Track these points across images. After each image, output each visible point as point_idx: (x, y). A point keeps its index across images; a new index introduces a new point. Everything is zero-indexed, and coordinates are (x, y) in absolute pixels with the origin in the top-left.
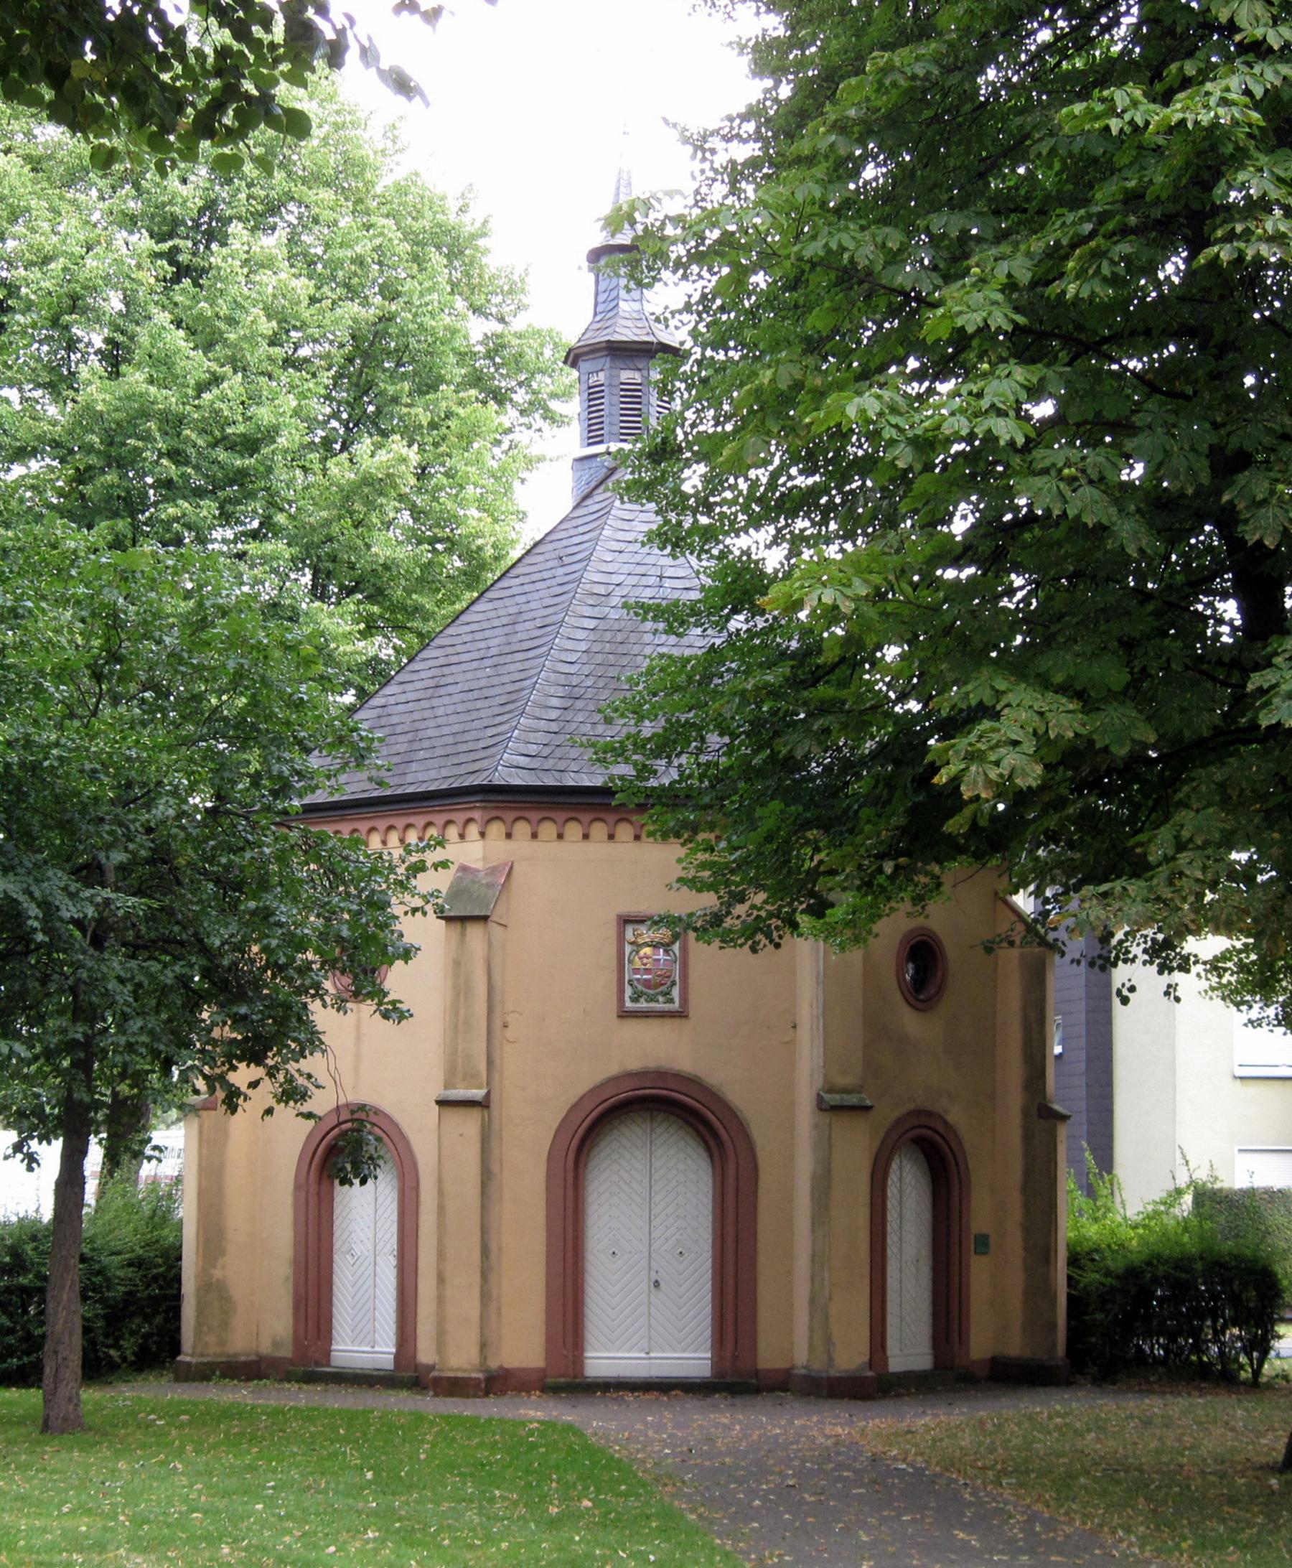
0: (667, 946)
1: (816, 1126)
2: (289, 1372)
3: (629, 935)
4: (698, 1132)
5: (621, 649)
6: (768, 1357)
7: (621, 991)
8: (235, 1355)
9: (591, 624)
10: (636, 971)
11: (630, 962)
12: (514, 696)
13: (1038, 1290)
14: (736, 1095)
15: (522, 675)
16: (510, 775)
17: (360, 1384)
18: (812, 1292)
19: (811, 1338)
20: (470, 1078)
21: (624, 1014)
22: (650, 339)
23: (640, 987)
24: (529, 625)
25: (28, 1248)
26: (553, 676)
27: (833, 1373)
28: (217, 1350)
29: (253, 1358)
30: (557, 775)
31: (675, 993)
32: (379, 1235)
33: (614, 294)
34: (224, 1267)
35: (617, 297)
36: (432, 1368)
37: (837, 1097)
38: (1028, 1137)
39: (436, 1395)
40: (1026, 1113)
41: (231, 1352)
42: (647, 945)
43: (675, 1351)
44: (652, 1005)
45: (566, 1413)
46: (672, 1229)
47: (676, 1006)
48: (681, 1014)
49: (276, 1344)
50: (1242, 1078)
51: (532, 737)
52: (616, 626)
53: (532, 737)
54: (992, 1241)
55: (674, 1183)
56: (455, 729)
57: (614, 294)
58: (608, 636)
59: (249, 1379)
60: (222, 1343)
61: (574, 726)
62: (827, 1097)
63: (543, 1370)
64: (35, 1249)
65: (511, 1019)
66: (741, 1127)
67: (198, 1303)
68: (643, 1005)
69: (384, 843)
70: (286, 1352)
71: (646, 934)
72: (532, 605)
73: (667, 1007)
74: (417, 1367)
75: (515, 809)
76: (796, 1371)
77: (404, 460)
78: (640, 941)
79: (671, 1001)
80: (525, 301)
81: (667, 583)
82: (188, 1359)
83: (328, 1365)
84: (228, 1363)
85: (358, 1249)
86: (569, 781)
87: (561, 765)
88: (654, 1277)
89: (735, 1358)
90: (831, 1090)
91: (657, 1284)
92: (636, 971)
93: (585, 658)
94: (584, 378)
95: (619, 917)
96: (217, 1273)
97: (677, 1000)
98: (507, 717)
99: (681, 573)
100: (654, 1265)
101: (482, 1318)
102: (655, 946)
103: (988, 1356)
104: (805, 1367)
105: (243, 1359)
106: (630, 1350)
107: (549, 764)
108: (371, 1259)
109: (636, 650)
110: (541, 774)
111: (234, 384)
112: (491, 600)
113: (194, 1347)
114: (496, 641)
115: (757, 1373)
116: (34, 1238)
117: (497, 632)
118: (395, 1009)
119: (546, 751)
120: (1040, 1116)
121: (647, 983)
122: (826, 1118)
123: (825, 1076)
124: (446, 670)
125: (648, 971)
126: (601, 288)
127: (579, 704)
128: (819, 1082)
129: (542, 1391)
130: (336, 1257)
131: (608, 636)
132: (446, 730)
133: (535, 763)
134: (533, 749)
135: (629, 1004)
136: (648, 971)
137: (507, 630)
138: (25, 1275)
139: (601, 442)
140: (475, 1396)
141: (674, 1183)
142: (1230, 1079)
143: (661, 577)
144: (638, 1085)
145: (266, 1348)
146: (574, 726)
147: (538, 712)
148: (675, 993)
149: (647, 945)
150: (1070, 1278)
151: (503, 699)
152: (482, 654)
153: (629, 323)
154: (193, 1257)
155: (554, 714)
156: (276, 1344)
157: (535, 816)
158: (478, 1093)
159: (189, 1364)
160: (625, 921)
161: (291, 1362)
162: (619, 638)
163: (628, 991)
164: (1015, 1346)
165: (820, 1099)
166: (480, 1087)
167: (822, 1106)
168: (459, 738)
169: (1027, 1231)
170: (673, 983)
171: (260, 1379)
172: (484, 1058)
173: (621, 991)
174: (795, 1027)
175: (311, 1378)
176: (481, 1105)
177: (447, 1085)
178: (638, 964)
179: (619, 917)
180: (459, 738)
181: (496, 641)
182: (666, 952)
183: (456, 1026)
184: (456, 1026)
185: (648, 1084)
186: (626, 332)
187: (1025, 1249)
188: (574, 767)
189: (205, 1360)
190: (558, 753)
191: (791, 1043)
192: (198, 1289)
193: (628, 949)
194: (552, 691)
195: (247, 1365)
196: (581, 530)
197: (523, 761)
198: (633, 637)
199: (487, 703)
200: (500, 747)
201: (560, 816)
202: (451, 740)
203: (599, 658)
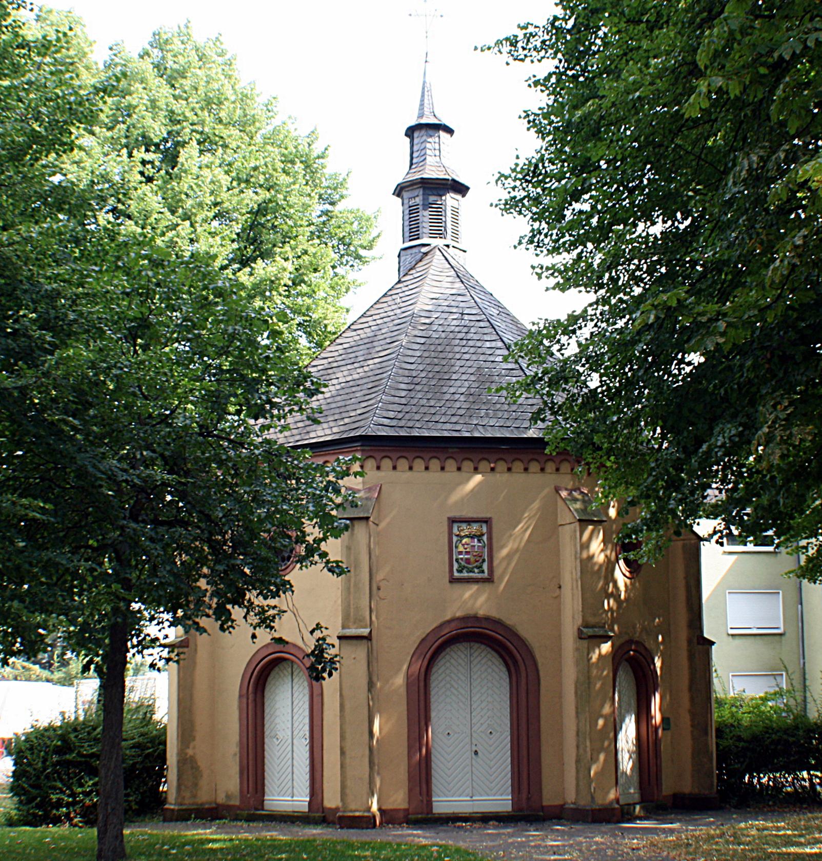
0: (479, 537)
1: (577, 649)
2: (237, 815)
3: (455, 531)
4: (501, 656)
5: (441, 355)
6: (549, 798)
7: (451, 566)
8: (202, 804)
9: (422, 340)
10: (460, 553)
11: (456, 547)
12: (377, 383)
13: (699, 751)
14: (526, 631)
15: (381, 371)
16: (378, 430)
17: (285, 822)
18: (578, 755)
19: (577, 785)
20: (359, 622)
21: (453, 580)
22: (447, 177)
23: (463, 563)
24: (382, 342)
25: (72, 736)
26: (401, 371)
27: (595, 807)
28: (191, 801)
29: (214, 805)
30: (408, 430)
31: (485, 567)
32: (295, 726)
33: (423, 152)
34: (194, 748)
35: (425, 154)
36: (337, 809)
37: (591, 630)
38: (691, 657)
39: (341, 828)
40: (690, 642)
41: (200, 802)
42: (466, 536)
43: (488, 795)
44: (471, 574)
45: (421, 837)
46: (486, 717)
47: (486, 575)
48: (489, 580)
49: (228, 797)
50: (733, 635)
51: (391, 407)
52: (437, 342)
53: (391, 407)
54: (672, 720)
55: (485, 688)
56: (339, 404)
57: (423, 152)
58: (432, 348)
59: (213, 819)
60: (194, 796)
61: (416, 400)
62: (585, 630)
63: (406, 810)
64: (76, 737)
65: (382, 584)
66: (529, 652)
67: (178, 771)
68: (465, 574)
69: (362, 467)
70: (236, 802)
71: (466, 530)
72: (383, 331)
73: (480, 576)
74: (324, 809)
75: (383, 451)
76: (567, 806)
77: (285, 270)
78: (462, 534)
79: (483, 572)
80: (345, 192)
81: (466, 317)
82: (172, 807)
83: (263, 809)
84: (197, 809)
85: (280, 735)
86: (415, 433)
87: (410, 424)
88: (474, 748)
89: (528, 799)
90: (586, 627)
91: (476, 753)
92: (460, 553)
93: (419, 360)
94: (406, 201)
95: (449, 518)
96: (190, 752)
97: (486, 571)
98: (373, 395)
99: (474, 312)
100: (474, 742)
101: (370, 776)
102: (472, 537)
103: (671, 793)
104: (574, 803)
105: (207, 806)
106: (460, 796)
107: (402, 423)
108: (290, 741)
109: (450, 356)
110: (397, 429)
111: (185, 228)
112: (355, 330)
113: (176, 799)
114: (361, 353)
115: (543, 808)
116: (75, 730)
117: (361, 347)
118: (338, 566)
119: (400, 415)
120: (699, 643)
121: (468, 561)
122: (585, 643)
123: (583, 617)
124: (330, 371)
125: (467, 553)
126: (415, 148)
127: (418, 388)
128: (580, 622)
129: (407, 823)
130: (266, 740)
131: (432, 348)
132: (333, 405)
133: (394, 423)
134: (391, 415)
135: (456, 574)
136: (467, 553)
137: (368, 346)
138: (70, 754)
139: (418, 238)
140: (367, 828)
141: (485, 688)
142: (725, 635)
143: (462, 314)
144: (463, 626)
145: (221, 799)
146: (416, 400)
147: (393, 392)
148: (485, 567)
149: (466, 536)
150: (717, 744)
151: (370, 386)
152: (352, 360)
153: (433, 168)
154: (175, 742)
155: (403, 394)
156: (228, 797)
157: (395, 455)
158: (365, 632)
159: (173, 810)
160: (453, 521)
161: (238, 808)
162: (440, 348)
163: (456, 566)
164: (687, 786)
165: (580, 631)
166: (365, 627)
167: (581, 636)
168: (342, 410)
169: (693, 714)
170: (484, 561)
171: (220, 819)
172: (368, 609)
173: (451, 566)
174: (560, 587)
175: (251, 818)
176: (368, 638)
177: (343, 627)
178: (461, 549)
179: (449, 518)
180: (342, 410)
181: (361, 353)
182: (479, 541)
183: (349, 589)
184: (349, 589)
185: (470, 625)
186: (431, 172)
187: (692, 726)
188: (418, 425)
189: (184, 807)
190: (407, 416)
191: (558, 597)
192: (178, 762)
193: (455, 539)
194: (401, 379)
195: (210, 810)
196: (411, 287)
197: (386, 421)
198: (448, 349)
199: (359, 388)
200: (371, 413)
201: (410, 455)
202: (337, 411)
203: (428, 361)
